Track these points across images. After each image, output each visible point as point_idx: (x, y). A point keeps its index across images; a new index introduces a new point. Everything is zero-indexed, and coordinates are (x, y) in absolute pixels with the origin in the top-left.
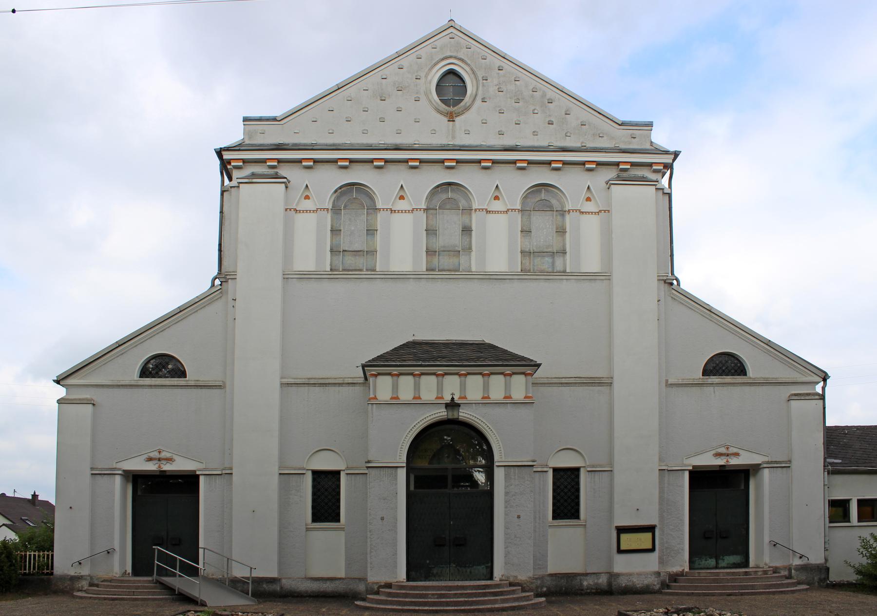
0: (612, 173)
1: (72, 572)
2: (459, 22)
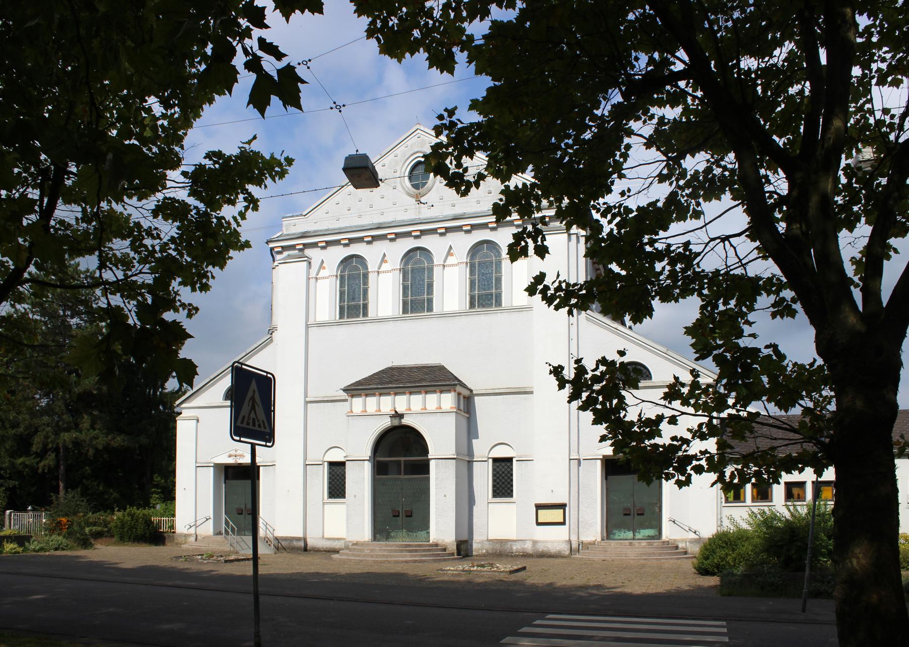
1: (186, 532)
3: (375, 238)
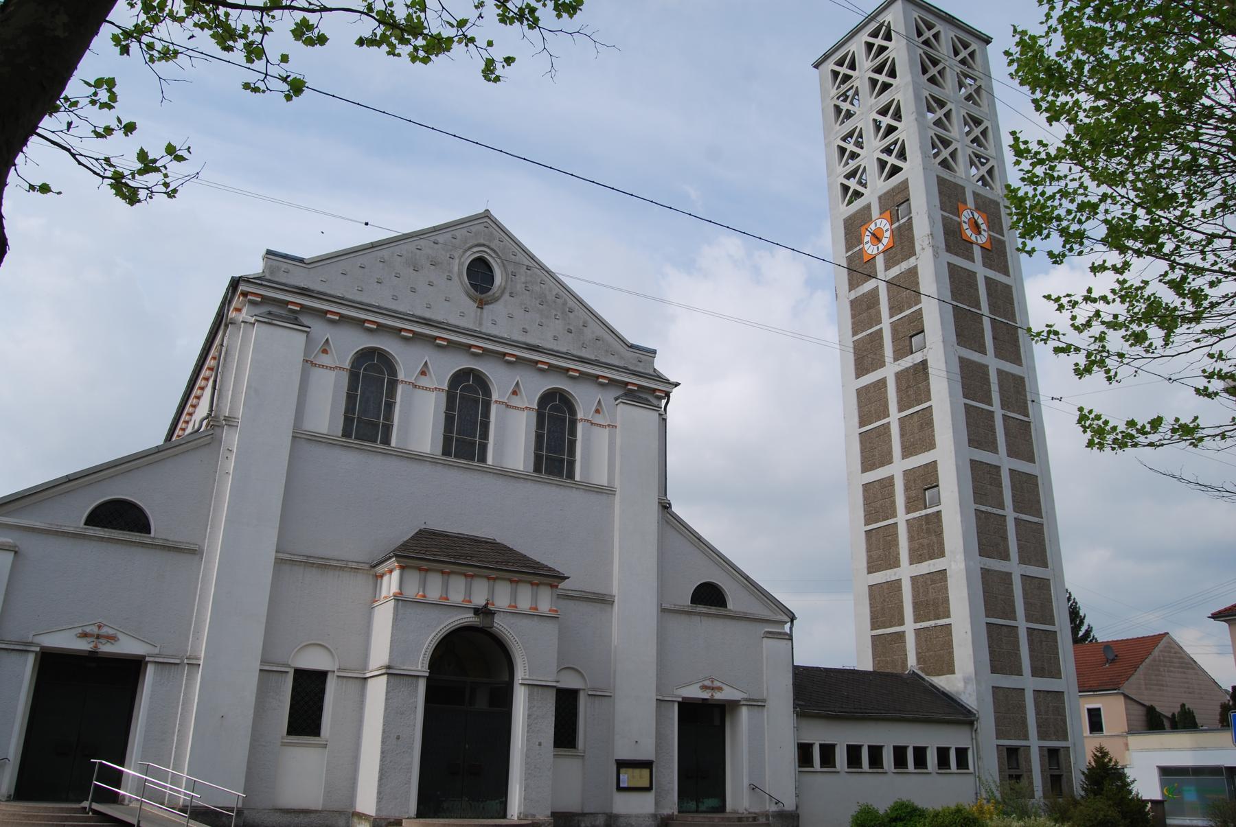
0: (620, 392)
2: (495, 213)
3: (417, 337)
